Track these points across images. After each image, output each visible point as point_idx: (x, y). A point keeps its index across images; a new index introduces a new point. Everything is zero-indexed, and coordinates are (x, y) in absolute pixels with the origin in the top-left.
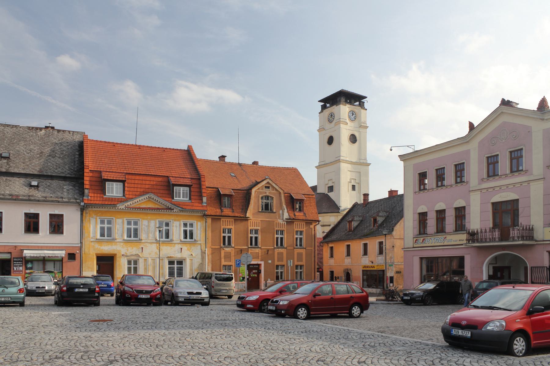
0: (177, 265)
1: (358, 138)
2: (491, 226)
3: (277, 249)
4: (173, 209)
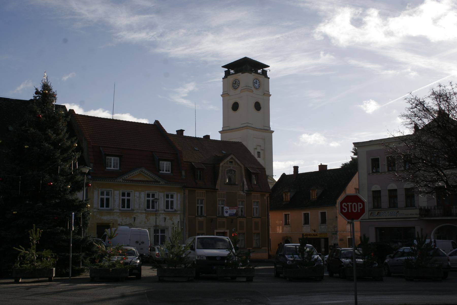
0: (161, 233)
1: (262, 106)
2: (436, 204)
3: (239, 219)
4: (159, 182)
